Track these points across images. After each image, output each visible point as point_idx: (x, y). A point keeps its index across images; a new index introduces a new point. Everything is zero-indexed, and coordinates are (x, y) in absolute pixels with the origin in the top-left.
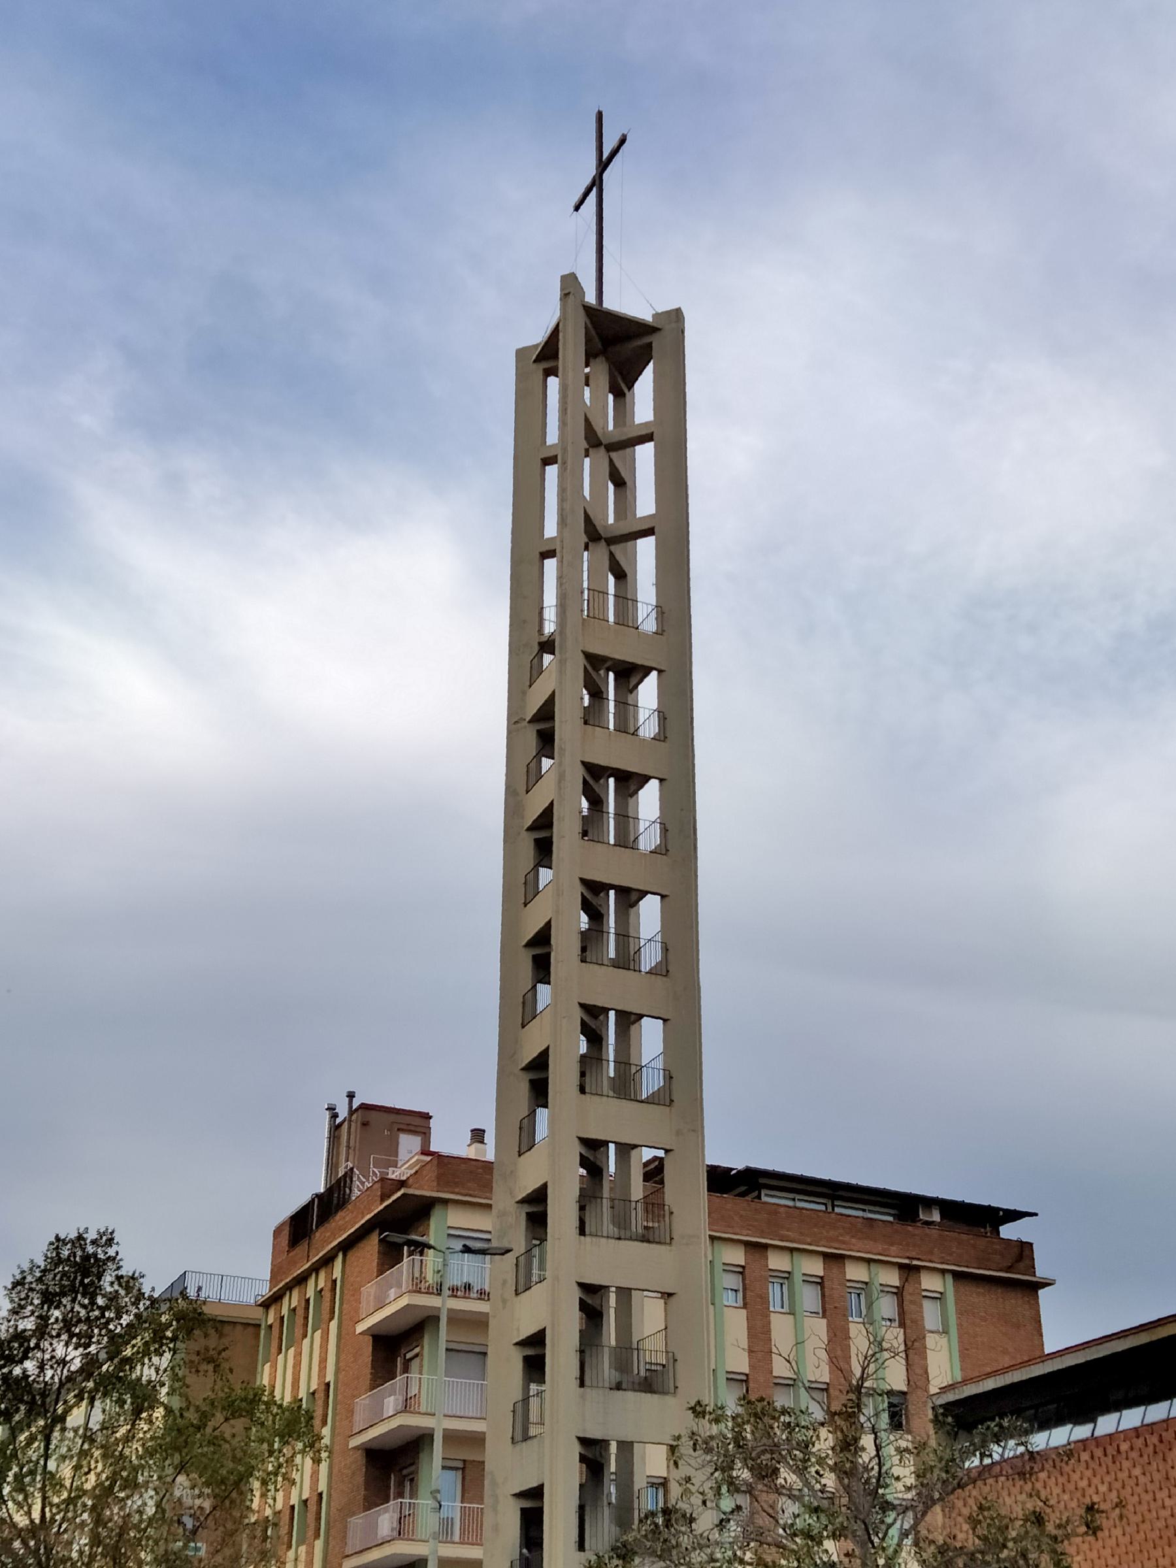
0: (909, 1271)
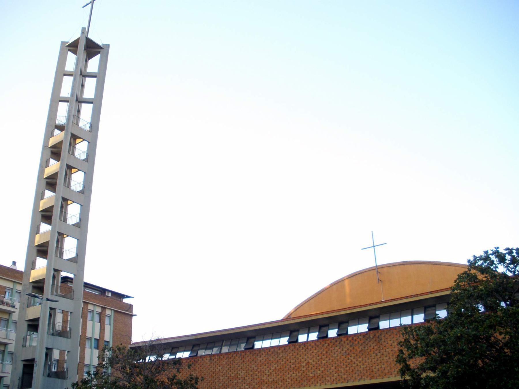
0: (104, 309)
